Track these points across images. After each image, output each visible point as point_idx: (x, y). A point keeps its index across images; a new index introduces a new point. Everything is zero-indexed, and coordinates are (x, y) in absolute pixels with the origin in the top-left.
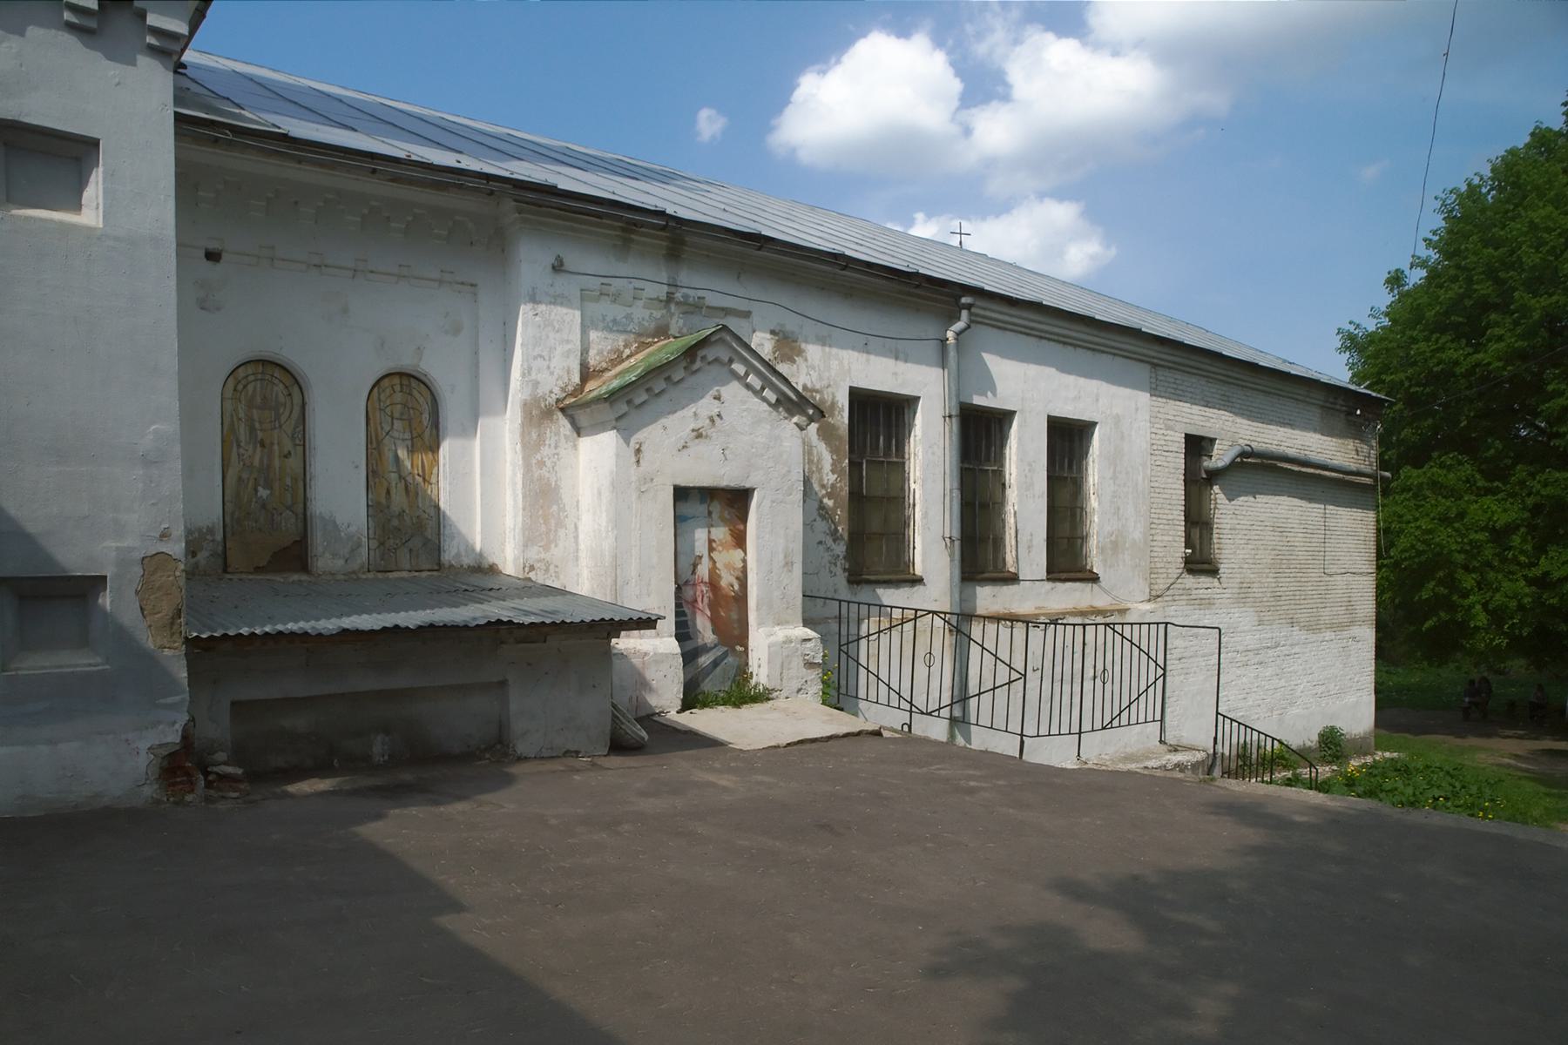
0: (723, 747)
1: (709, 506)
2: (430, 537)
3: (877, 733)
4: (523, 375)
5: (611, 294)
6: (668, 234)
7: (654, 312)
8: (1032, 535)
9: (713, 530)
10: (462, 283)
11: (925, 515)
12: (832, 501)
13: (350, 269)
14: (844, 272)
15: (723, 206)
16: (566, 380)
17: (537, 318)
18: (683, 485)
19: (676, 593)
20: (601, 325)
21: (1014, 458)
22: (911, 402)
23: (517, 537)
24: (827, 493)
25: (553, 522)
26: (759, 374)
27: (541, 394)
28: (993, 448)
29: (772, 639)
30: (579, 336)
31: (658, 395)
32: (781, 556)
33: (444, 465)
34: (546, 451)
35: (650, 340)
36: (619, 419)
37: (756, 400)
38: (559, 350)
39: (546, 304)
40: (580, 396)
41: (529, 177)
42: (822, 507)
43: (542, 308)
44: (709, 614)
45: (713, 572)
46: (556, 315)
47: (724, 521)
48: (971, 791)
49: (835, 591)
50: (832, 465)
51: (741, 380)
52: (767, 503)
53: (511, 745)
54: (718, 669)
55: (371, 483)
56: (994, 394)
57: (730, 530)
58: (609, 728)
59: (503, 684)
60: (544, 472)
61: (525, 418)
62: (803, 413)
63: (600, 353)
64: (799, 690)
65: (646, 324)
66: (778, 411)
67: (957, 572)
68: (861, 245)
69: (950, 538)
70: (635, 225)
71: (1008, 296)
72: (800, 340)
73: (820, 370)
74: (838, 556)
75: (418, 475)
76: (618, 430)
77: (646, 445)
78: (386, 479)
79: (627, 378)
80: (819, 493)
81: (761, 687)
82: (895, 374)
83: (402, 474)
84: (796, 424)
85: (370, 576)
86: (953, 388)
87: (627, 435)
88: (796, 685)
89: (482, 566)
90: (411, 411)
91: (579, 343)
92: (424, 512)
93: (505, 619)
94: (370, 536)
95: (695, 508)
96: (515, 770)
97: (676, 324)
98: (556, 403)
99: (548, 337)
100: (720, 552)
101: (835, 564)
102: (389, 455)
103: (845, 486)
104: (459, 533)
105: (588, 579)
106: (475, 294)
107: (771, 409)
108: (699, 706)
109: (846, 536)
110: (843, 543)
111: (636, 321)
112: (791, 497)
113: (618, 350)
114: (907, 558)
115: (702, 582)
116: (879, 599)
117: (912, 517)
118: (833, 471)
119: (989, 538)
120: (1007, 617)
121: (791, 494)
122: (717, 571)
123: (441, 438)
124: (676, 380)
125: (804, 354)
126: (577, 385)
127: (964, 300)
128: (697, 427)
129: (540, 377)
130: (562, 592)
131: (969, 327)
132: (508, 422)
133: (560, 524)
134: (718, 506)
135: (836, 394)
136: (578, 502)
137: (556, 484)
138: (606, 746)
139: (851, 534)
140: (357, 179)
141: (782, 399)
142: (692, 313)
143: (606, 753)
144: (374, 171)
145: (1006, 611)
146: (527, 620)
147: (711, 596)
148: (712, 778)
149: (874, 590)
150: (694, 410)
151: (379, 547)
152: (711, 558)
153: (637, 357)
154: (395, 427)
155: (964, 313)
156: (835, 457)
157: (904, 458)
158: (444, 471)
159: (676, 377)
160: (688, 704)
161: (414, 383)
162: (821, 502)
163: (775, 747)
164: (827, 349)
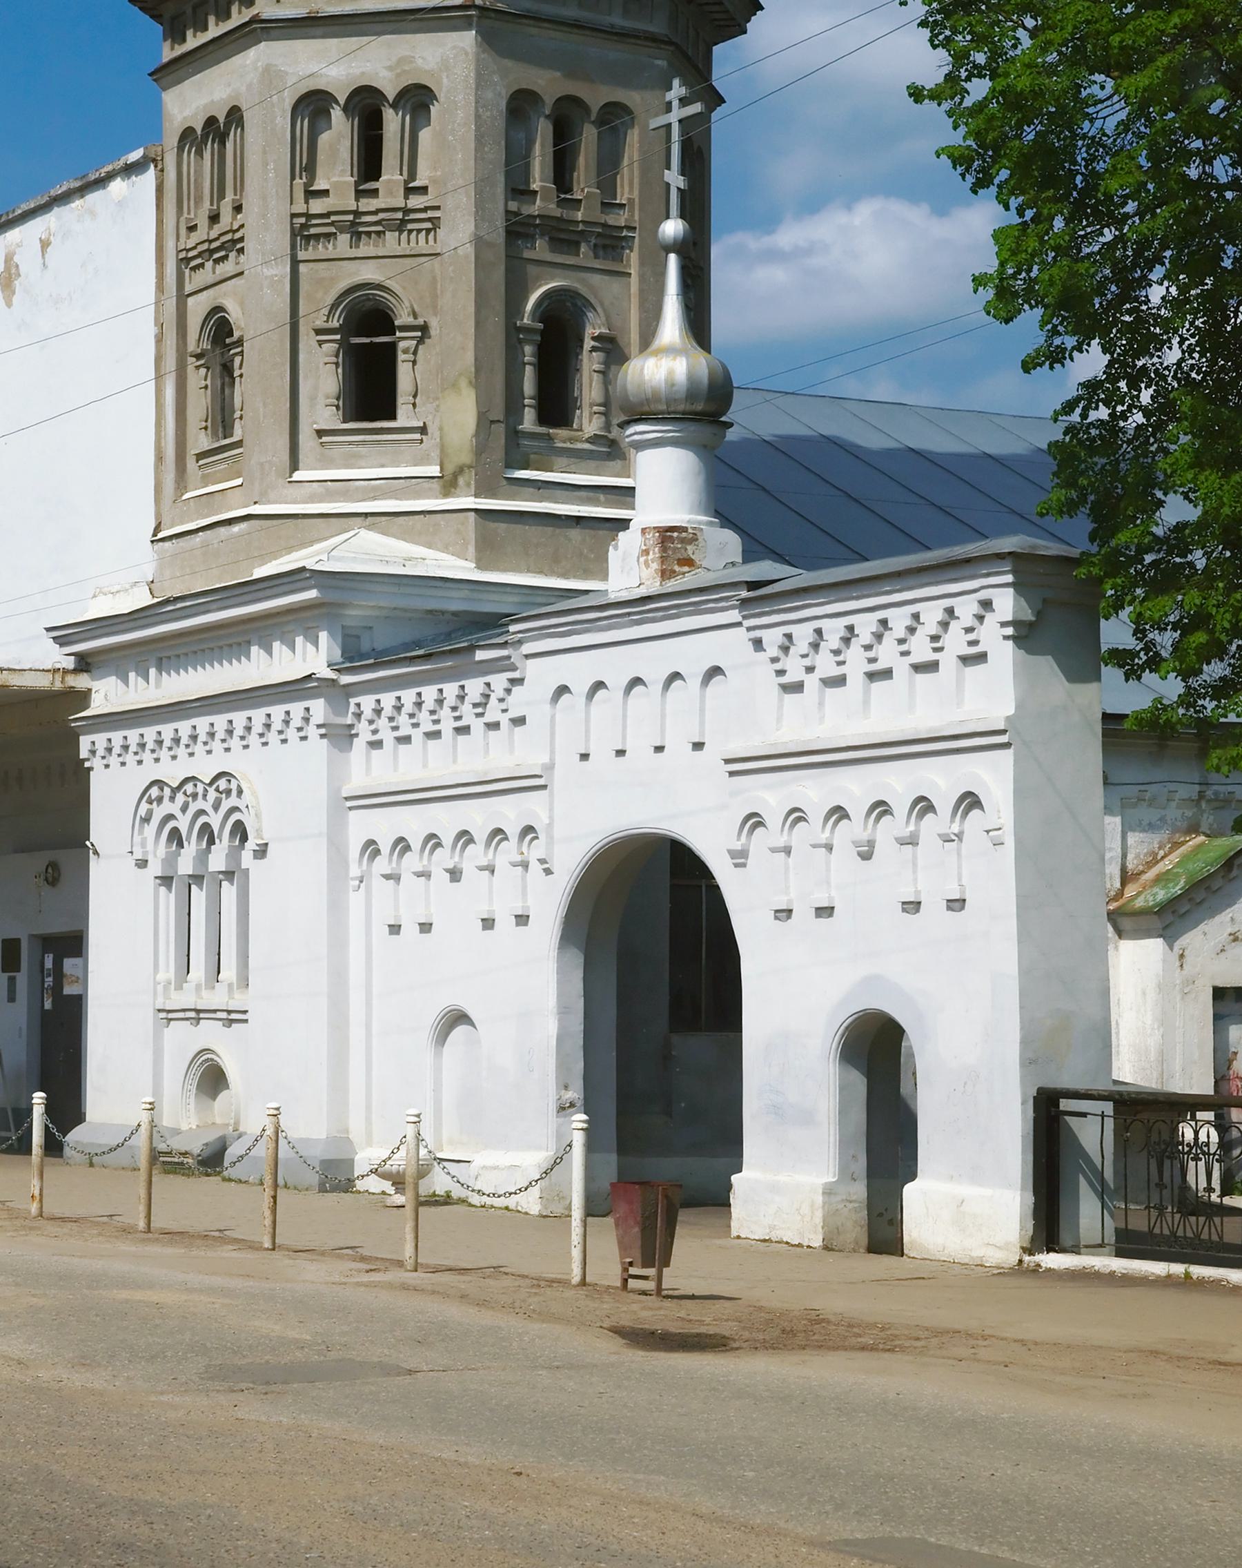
31: (1200, 903)
35: (1182, 839)
36: (1165, 928)
63: (1137, 856)
65: (1179, 824)
87: (1170, 939)
91: (1120, 850)
111: (1169, 822)
142: (1222, 808)
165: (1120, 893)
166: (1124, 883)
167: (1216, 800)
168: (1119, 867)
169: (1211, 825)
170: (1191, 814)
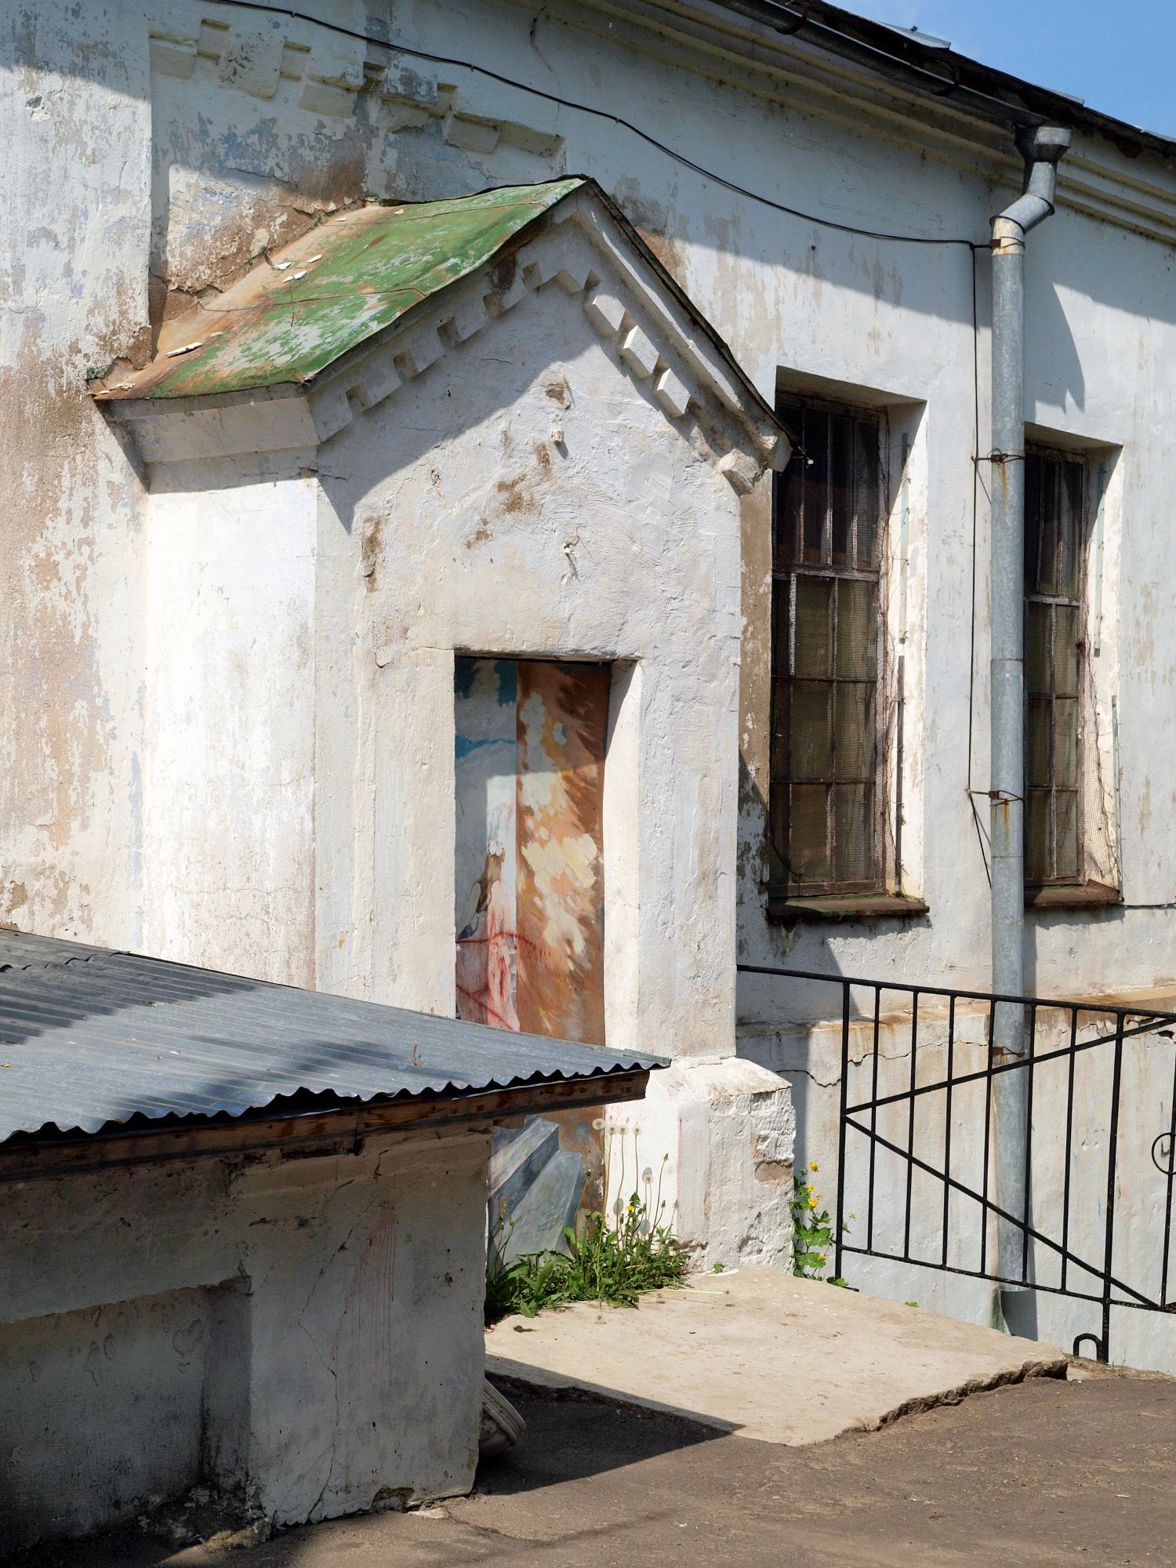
5: (223, 54)
7: (325, 119)
8: (1148, 783)
9: (528, 779)
11: (931, 730)
14: (787, 40)
16: (114, 315)
17: (39, 115)
20: (197, 149)
21: (1112, 573)
25: (76, 750)
27: (47, 354)
30: (146, 177)
32: (693, 854)
34: (59, 531)
37: (642, 402)
39: (62, 72)
43: (51, 82)
47: (560, 757)
51: (610, 340)
52: (664, 700)
53: (251, 1490)
54: (535, 1187)
57: (567, 779)
60: (53, 596)
63: (195, 234)
64: (744, 1242)
65: (308, 155)
66: (688, 438)
69: (994, 794)
72: (670, 230)
76: (322, 482)
77: (392, 527)
82: (874, 335)
88: (735, 1229)
91: (147, 200)
103: (764, 647)
107: (671, 430)
108: (523, 1305)
111: (283, 143)
112: (715, 683)
113: (240, 229)
115: (501, 933)
116: (834, 964)
121: (714, 677)
122: (537, 900)
124: (466, 335)
128: (508, 480)
133: (95, 757)
134: (542, 709)
136: (141, 689)
137: (86, 635)
138: (469, 1466)
141: (701, 402)
142: (419, 130)
143: (468, 1489)
147: (523, 975)
149: (823, 943)
150: (503, 425)
152: (523, 861)
155: (1041, 172)
164: (730, 259)
165: (147, 346)
166: (157, 313)
167: (408, 100)
168: (143, 260)
169: (391, 178)
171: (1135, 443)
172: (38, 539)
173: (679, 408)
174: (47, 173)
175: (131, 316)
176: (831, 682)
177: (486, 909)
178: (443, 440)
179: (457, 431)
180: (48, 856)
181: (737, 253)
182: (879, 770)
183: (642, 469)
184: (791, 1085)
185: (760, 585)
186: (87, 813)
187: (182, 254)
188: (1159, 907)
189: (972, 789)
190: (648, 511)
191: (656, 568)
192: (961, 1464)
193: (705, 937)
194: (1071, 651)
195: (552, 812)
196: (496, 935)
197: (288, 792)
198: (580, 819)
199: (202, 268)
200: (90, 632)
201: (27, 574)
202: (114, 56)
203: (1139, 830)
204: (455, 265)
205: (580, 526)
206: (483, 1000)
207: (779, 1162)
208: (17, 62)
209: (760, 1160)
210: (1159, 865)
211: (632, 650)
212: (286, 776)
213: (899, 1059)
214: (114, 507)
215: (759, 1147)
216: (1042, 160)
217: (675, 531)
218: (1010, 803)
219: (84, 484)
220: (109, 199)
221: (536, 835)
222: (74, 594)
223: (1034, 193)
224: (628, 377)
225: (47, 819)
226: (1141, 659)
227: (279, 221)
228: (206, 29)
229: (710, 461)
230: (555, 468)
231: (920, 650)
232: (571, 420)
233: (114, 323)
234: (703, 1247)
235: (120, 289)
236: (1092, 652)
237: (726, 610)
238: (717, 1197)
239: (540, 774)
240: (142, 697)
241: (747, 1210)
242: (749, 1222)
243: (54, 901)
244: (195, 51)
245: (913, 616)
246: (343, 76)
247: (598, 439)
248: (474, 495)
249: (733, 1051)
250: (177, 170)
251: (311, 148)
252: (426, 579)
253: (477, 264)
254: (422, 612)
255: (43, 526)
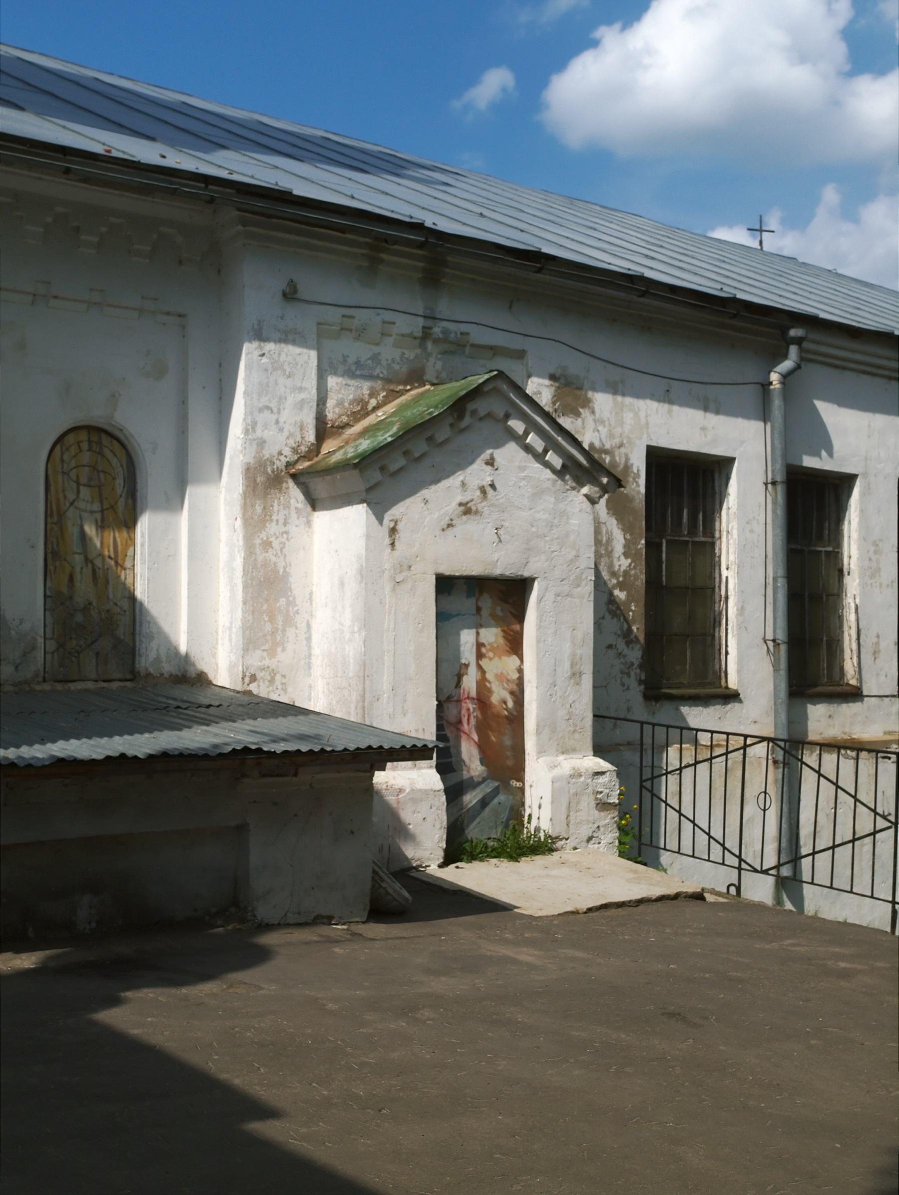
0: (510, 912)
1: (477, 600)
2: (122, 637)
3: (699, 897)
4: (246, 432)
6: (425, 253)
7: (406, 351)
8: (878, 637)
9: (483, 631)
10: (168, 313)
11: (741, 611)
12: (625, 593)
13: (29, 293)
14: (642, 300)
15: (479, 210)
16: (299, 439)
18: (448, 573)
19: (437, 712)
20: (341, 368)
21: (855, 535)
22: (723, 465)
23: (234, 637)
24: (619, 582)
25: (280, 620)
26: (541, 432)
28: (827, 524)
29: (557, 772)
32: (567, 665)
33: (142, 545)
34: (272, 528)
35: (401, 387)
36: (369, 490)
37: (538, 465)
38: (291, 399)
39: (275, 342)
40: (316, 459)
41: (252, 177)
42: (612, 600)
43: (270, 346)
44: (476, 738)
45: (482, 683)
46: (287, 355)
47: (498, 621)
48: (845, 974)
49: (629, 710)
50: (625, 546)
51: (520, 440)
52: (550, 596)
53: (250, 909)
54: (487, 810)
55: (51, 567)
56: (831, 454)
57: (503, 631)
58: (369, 885)
59: (242, 829)
60: (270, 555)
61: (247, 486)
62: (595, 482)
63: (340, 403)
64: (590, 839)
65: (397, 367)
66: (563, 480)
67: (783, 686)
68: (653, 258)
69: (774, 641)
70: (386, 241)
71: (859, 328)
72: (586, 387)
73: (610, 425)
74: (632, 664)
75: (110, 557)
76: (369, 505)
78: (68, 562)
79: (381, 438)
80: (609, 582)
81: (542, 835)
82: (704, 429)
83: (90, 557)
84: (586, 496)
85: (47, 687)
86: (778, 445)
87: (379, 510)
88: (586, 832)
89: (189, 675)
90: (102, 475)
91: (314, 391)
92: (116, 604)
93: (253, 747)
94: (47, 636)
95: (461, 603)
96: (268, 939)
97: (433, 366)
98: (286, 466)
99: (276, 384)
100: (491, 659)
101: (628, 675)
102: (72, 531)
103: (641, 573)
104: (160, 631)
105: (324, 692)
106: (184, 327)
107: (555, 477)
108: (465, 858)
109: (642, 638)
110: (638, 646)
111: (384, 363)
112: (580, 589)
113: (362, 400)
114: (717, 667)
115: (468, 698)
116: (684, 719)
117: (724, 613)
118: (626, 555)
119: (822, 640)
120: (847, 745)
121: (578, 586)
122: (487, 684)
123: (138, 509)
124: (440, 441)
125: (591, 404)
126: (312, 444)
127: (793, 333)
128: (464, 501)
129: (267, 434)
130: (306, 712)
131: (798, 367)
132: (223, 490)
133: (289, 621)
135: (630, 456)
136: (311, 594)
137: (285, 571)
139: (648, 635)
140: (40, 179)
141: (569, 464)
142: (452, 353)
143: (364, 919)
144: (67, 171)
145: (846, 737)
146: (279, 748)
147: (480, 716)
148: (509, 952)
149: (677, 709)
150: (461, 478)
151: (57, 649)
152: (479, 667)
153: (385, 409)
154: (82, 496)
155: (793, 350)
156: (628, 537)
157: (713, 536)
158: (142, 553)
159: (440, 437)
160: (451, 857)
161: (105, 440)
162: (611, 594)
163: (572, 913)
164: (619, 398)
167: (445, 340)
170: (412, 357)
171: (866, 473)
172: (263, 532)
173: (555, 465)
174: (267, 385)
175: (306, 439)
176: (687, 588)
177: (460, 687)
178: (430, 485)
179: (437, 481)
180: (267, 662)
181: (623, 395)
182: (717, 630)
183: (538, 494)
184: (616, 769)
185: (638, 545)
186: (285, 645)
187: (333, 412)
188: (887, 696)
189: (767, 638)
190: (541, 513)
191: (546, 538)
192: (598, 926)
193: (574, 702)
194: (836, 573)
195: (495, 645)
196: (465, 699)
197: (357, 635)
198: (510, 648)
199: (343, 417)
200: (287, 569)
201: (258, 546)
202: (300, 333)
203: (873, 659)
204: (432, 412)
205: (503, 520)
206: (459, 726)
207: (610, 803)
208: (254, 339)
209: (599, 802)
210: (886, 676)
211: (532, 574)
212: (356, 629)
213: (717, 764)
214: (298, 518)
215: (598, 796)
216: (793, 344)
217: (556, 521)
218: (781, 645)
219: (284, 509)
220: (297, 391)
221: (487, 655)
222: (279, 554)
223: (790, 359)
224: (530, 455)
225: (266, 647)
226: (872, 576)
227: (382, 395)
228: (345, 319)
229: (577, 490)
230: (489, 496)
231: (734, 573)
232: (498, 474)
233: (298, 442)
234: (567, 839)
235: (302, 428)
236: (846, 573)
237: (585, 556)
238: (574, 817)
239: (488, 629)
240: (311, 597)
241: (591, 824)
242: (593, 829)
243: (269, 681)
244: (339, 328)
245: (732, 557)
246: (412, 333)
247: (513, 482)
248: (446, 509)
249: (592, 753)
250: (332, 378)
251: (398, 364)
252: (421, 545)
253: (441, 411)
254: (418, 559)
255: (265, 526)
